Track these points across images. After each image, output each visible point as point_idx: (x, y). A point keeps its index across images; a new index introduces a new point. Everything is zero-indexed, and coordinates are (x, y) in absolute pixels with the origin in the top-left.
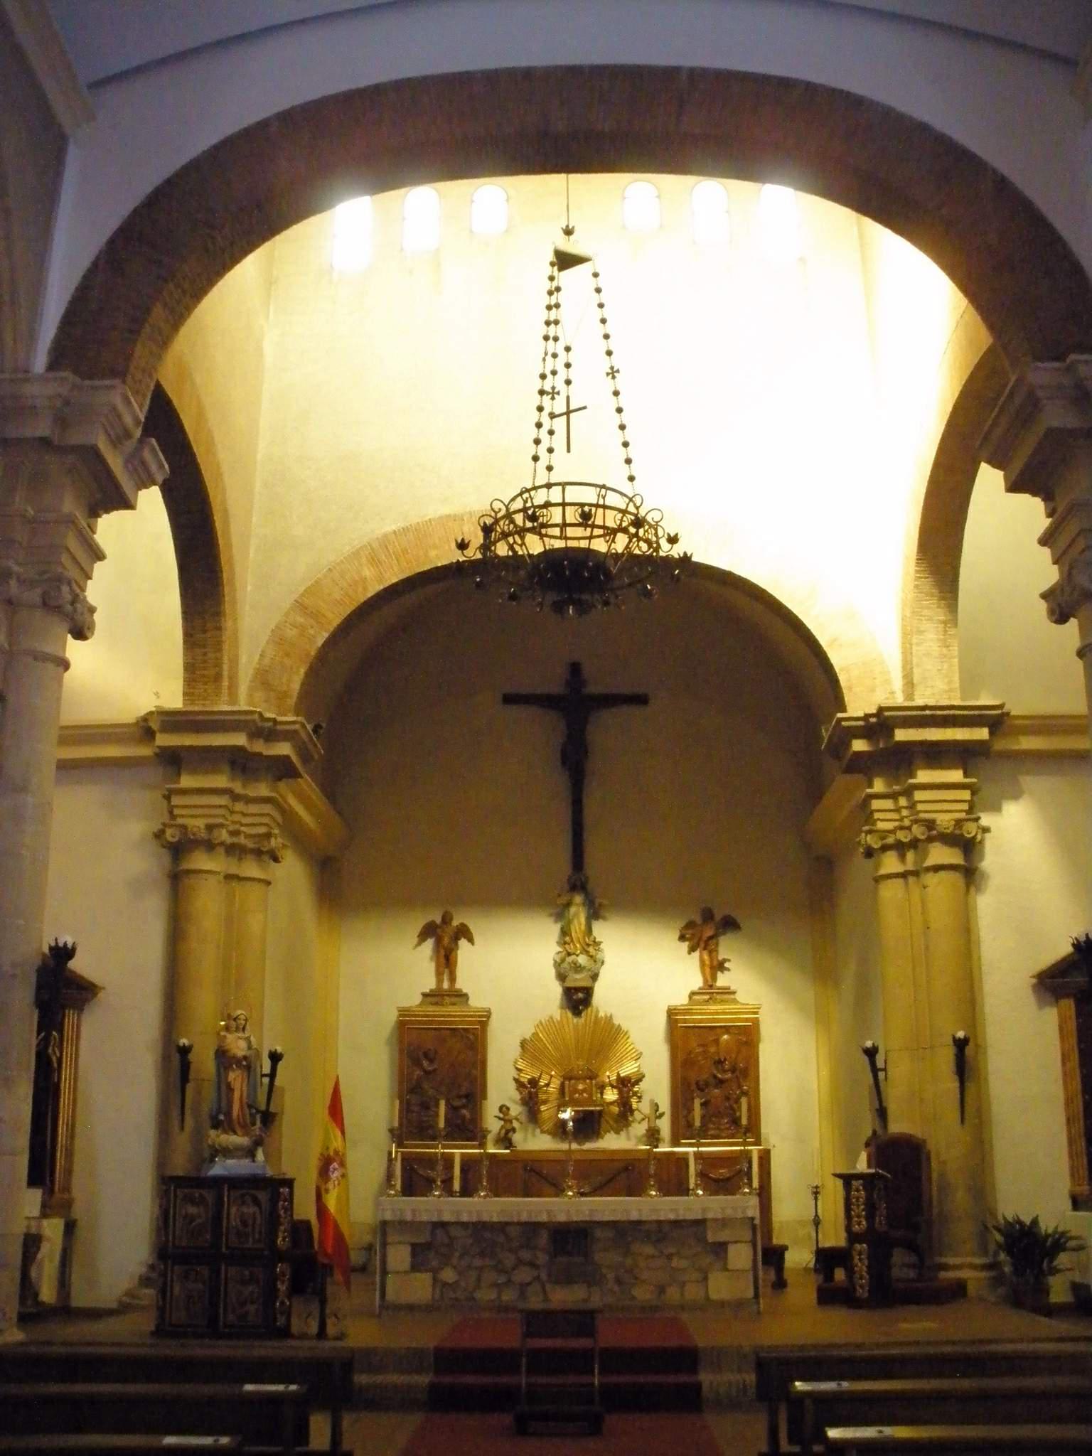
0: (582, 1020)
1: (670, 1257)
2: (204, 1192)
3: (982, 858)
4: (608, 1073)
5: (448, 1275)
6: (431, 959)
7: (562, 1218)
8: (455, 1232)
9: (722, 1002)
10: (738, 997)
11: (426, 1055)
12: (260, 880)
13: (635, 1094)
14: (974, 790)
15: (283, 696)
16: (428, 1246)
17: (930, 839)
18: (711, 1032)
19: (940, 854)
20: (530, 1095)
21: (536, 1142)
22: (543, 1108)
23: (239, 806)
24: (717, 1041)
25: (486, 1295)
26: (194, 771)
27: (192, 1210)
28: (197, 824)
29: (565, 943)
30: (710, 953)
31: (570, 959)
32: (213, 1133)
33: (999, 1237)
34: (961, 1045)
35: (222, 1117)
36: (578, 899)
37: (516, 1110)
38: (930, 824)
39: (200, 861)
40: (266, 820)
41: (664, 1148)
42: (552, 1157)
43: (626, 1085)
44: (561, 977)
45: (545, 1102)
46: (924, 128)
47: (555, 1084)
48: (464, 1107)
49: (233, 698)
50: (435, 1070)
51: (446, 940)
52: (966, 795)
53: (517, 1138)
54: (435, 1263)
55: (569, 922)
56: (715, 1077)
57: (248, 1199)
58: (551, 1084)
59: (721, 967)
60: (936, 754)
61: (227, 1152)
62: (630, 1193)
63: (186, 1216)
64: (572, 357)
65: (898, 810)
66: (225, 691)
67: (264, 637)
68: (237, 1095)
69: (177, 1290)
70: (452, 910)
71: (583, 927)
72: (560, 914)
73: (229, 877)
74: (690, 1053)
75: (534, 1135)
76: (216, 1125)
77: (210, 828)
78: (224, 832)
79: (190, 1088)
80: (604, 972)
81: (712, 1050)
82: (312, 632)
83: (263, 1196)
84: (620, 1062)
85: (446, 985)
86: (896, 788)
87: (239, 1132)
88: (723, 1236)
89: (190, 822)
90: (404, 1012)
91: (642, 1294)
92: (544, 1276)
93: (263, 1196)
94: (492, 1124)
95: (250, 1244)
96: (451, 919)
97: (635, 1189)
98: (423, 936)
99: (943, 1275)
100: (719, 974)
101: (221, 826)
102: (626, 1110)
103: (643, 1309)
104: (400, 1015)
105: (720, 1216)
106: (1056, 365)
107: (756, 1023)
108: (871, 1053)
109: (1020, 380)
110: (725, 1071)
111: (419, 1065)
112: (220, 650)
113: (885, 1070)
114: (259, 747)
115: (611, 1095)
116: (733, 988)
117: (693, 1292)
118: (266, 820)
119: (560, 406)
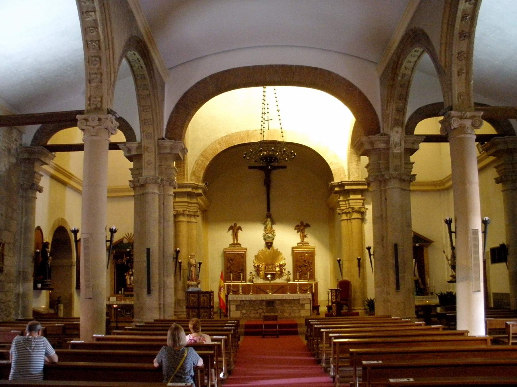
0: (270, 250)
1: (292, 307)
2: (196, 295)
3: (366, 215)
4: (277, 264)
5: (244, 311)
6: (232, 235)
7: (268, 299)
8: (245, 302)
9: (307, 245)
10: (310, 244)
11: (231, 260)
12: (195, 222)
13: (284, 269)
14: (364, 200)
15: (199, 177)
16: (239, 305)
17: (353, 212)
18: (302, 253)
19: (355, 215)
20: (257, 270)
21: (259, 281)
22: (261, 272)
23: (190, 205)
24: (304, 255)
25: (252, 315)
26: (179, 197)
27: (193, 298)
28: (181, 210)
29: (266, 231)
30: (303, 233)
31: (267, 235)
32: (188, 281)
33: (366, 303)
34: (359, 260)
35: (190, 278)
36: (269, 220)
37: (254, 273)
38: (353, 208)
39: (182, 218)
40: (196, 208)
41: (291, 282)
42: (263, 285)
43: (281, 266)
44: (265, 239)
45: (261, 271)
46: (344, 79)
47: (263, 267)
48: (241, 272)
49: (187, 181)
50: (233, 264)
51: (235, 231)
52: (362, 201)
53: (254, 280)
54: (241, 309)
55: (267, 225)
56: (304, 264)
57: (205, 296)
58: (262, 266)
59: (305, 236)
60: (355, 192)
61: (192, 286)
62: (283, 293)
63: (192, 300)
64: (268, 106)
65: (346, 204)
66: (186, 178)
67: (194, 163)
68: (193, 273)
69: (191, 314)
70: (237, 223)
71: (270, 227)
72: (264, 223)
73: (188, 222)
74: (298, 258)
75: (258, 279)
76: (189, 280)
77: (184, 211)
78: (187, 212)
79: (182, 271)
80: (276, 238)
81: (303, 257)
82: (205, 162)
83: (208, 295)
84: (280, 261)
85: (235, 242)
86: (345, 199)
87: (194, 281)
88: (303, 303)
89: (179, 209)
90: (225, 249)
91: (286, 315)
92: (265, 311)
93: (208, 295)
94: (248, 277)
95: (205, 305)
96: (237, 225)
97: (284, 292)
98: (229, 230)
99: (354, 311)
100: (305, 238)
101: (186, 210)
102: (281, 273)
103: (286, 318)
104: (224, 250)
105: (303, 298)
106: (367, 137)
107: (314, 251)
108: (339, 261)
109: (360, 139)
110: (306, 263)
111: (229, 262)
112: (184, 168)
113: (342, 265)
114: (195, 191)
115: (278, 269)
116: (308, 242)
117: (297, 314)
118: (196, 208)
119: (266, 119)
